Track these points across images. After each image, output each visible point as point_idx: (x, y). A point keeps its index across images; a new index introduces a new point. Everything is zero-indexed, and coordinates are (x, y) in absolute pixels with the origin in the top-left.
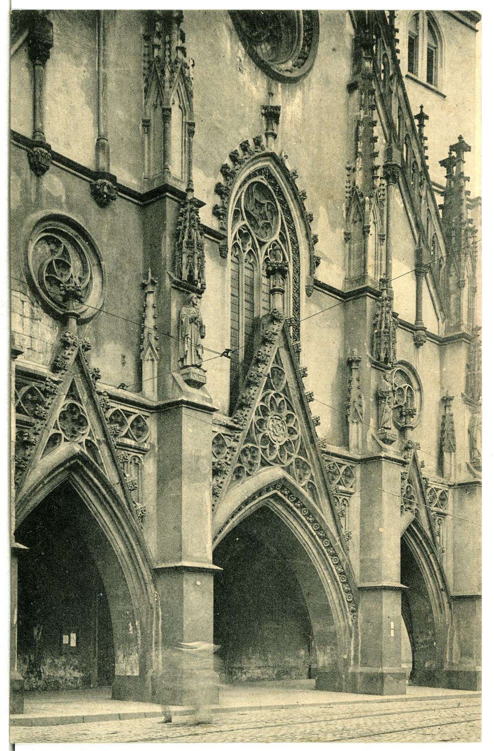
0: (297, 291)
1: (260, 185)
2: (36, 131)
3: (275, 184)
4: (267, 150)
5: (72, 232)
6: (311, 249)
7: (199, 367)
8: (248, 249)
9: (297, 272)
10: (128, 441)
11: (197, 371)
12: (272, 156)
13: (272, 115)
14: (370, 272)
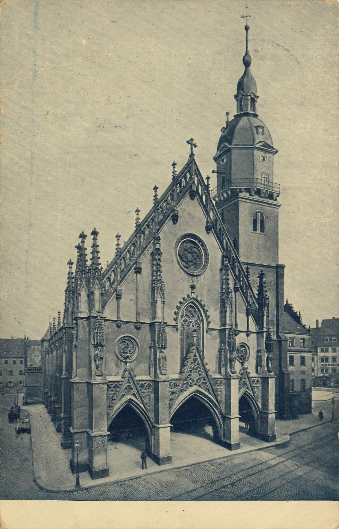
0: (203, 332)
1: (191, 307)
2: (118, 317)
3: (195, 304)
4: (191, 297)
5: (129, 339)
6: (207, 320)
7: (165, 370)
8: (187, 324)
9: (203, 327)
10: (145, 391)
11: (165, 371)
12: (194, 298)
13: (193, 287)
14: (228, 322)
